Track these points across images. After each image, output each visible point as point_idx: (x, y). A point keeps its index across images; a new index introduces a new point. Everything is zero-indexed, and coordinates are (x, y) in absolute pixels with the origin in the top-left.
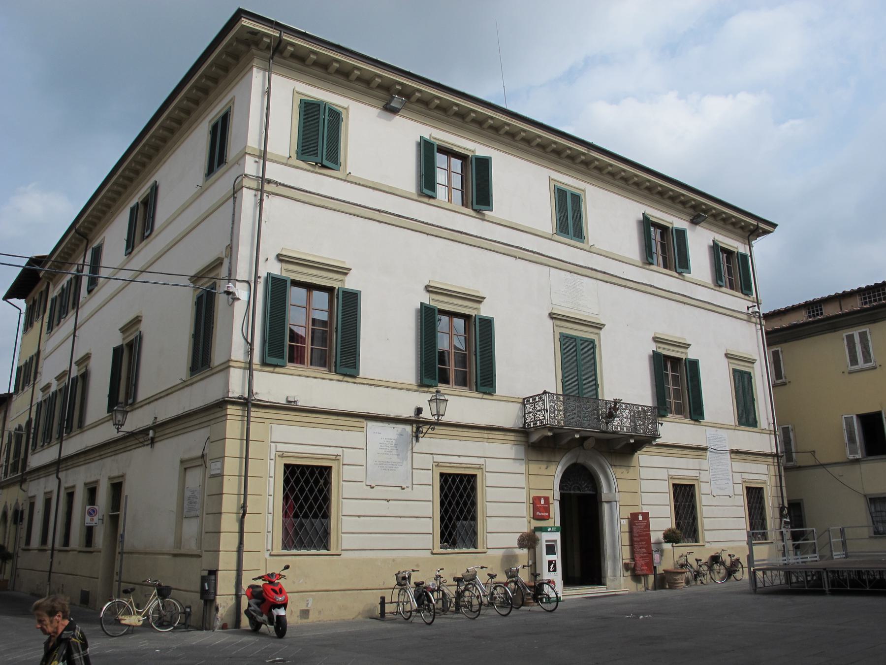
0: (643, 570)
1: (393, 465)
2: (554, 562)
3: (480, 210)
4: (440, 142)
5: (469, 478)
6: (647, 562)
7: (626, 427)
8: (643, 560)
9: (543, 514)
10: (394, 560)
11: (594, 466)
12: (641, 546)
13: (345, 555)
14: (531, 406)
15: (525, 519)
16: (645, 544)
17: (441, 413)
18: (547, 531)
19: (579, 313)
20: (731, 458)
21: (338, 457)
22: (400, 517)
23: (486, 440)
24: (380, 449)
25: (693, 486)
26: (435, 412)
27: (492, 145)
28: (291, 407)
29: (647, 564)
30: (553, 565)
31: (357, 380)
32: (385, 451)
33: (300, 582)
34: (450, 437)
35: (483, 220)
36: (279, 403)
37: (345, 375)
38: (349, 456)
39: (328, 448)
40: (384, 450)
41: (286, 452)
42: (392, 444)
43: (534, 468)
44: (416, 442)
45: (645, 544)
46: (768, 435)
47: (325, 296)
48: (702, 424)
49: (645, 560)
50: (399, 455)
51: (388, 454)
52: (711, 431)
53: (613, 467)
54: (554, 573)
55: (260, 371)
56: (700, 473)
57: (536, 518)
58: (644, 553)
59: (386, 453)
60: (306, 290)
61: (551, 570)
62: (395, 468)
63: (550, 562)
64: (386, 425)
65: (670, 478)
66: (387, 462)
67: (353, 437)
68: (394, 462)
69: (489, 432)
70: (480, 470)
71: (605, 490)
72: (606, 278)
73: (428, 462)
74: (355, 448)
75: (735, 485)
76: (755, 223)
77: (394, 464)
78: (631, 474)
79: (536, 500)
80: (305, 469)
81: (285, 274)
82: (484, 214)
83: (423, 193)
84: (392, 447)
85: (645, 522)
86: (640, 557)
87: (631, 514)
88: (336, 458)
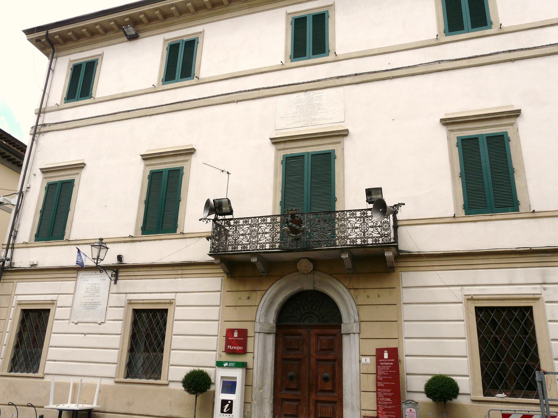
1: (94, 305)
4: (172, 41)
7: (372, 237)
8: (386, 414)
9: (235, 348)
14: (370, 234)
16: (391, 392)
21: (54, 302)
23: (180, 276)
24: (86, 292)
25: (530, 309)
30: (227, 405)
32: (89, 294)
38: (62, 300)
40: (89, 293)
45: (391, 392)
49: (389, 414)
51: (91, 296)
53: (352, 291)
57: (228, 352)
58: (389, 405)
61: (225, 411)
63: (224, 402)
66: (90, 303)
67: (67, 285)
68: (95, 303)
72: (357, 79)
76: (43, 33)
78: (386, 296)
79: (230, 332)
87: (377, 350)
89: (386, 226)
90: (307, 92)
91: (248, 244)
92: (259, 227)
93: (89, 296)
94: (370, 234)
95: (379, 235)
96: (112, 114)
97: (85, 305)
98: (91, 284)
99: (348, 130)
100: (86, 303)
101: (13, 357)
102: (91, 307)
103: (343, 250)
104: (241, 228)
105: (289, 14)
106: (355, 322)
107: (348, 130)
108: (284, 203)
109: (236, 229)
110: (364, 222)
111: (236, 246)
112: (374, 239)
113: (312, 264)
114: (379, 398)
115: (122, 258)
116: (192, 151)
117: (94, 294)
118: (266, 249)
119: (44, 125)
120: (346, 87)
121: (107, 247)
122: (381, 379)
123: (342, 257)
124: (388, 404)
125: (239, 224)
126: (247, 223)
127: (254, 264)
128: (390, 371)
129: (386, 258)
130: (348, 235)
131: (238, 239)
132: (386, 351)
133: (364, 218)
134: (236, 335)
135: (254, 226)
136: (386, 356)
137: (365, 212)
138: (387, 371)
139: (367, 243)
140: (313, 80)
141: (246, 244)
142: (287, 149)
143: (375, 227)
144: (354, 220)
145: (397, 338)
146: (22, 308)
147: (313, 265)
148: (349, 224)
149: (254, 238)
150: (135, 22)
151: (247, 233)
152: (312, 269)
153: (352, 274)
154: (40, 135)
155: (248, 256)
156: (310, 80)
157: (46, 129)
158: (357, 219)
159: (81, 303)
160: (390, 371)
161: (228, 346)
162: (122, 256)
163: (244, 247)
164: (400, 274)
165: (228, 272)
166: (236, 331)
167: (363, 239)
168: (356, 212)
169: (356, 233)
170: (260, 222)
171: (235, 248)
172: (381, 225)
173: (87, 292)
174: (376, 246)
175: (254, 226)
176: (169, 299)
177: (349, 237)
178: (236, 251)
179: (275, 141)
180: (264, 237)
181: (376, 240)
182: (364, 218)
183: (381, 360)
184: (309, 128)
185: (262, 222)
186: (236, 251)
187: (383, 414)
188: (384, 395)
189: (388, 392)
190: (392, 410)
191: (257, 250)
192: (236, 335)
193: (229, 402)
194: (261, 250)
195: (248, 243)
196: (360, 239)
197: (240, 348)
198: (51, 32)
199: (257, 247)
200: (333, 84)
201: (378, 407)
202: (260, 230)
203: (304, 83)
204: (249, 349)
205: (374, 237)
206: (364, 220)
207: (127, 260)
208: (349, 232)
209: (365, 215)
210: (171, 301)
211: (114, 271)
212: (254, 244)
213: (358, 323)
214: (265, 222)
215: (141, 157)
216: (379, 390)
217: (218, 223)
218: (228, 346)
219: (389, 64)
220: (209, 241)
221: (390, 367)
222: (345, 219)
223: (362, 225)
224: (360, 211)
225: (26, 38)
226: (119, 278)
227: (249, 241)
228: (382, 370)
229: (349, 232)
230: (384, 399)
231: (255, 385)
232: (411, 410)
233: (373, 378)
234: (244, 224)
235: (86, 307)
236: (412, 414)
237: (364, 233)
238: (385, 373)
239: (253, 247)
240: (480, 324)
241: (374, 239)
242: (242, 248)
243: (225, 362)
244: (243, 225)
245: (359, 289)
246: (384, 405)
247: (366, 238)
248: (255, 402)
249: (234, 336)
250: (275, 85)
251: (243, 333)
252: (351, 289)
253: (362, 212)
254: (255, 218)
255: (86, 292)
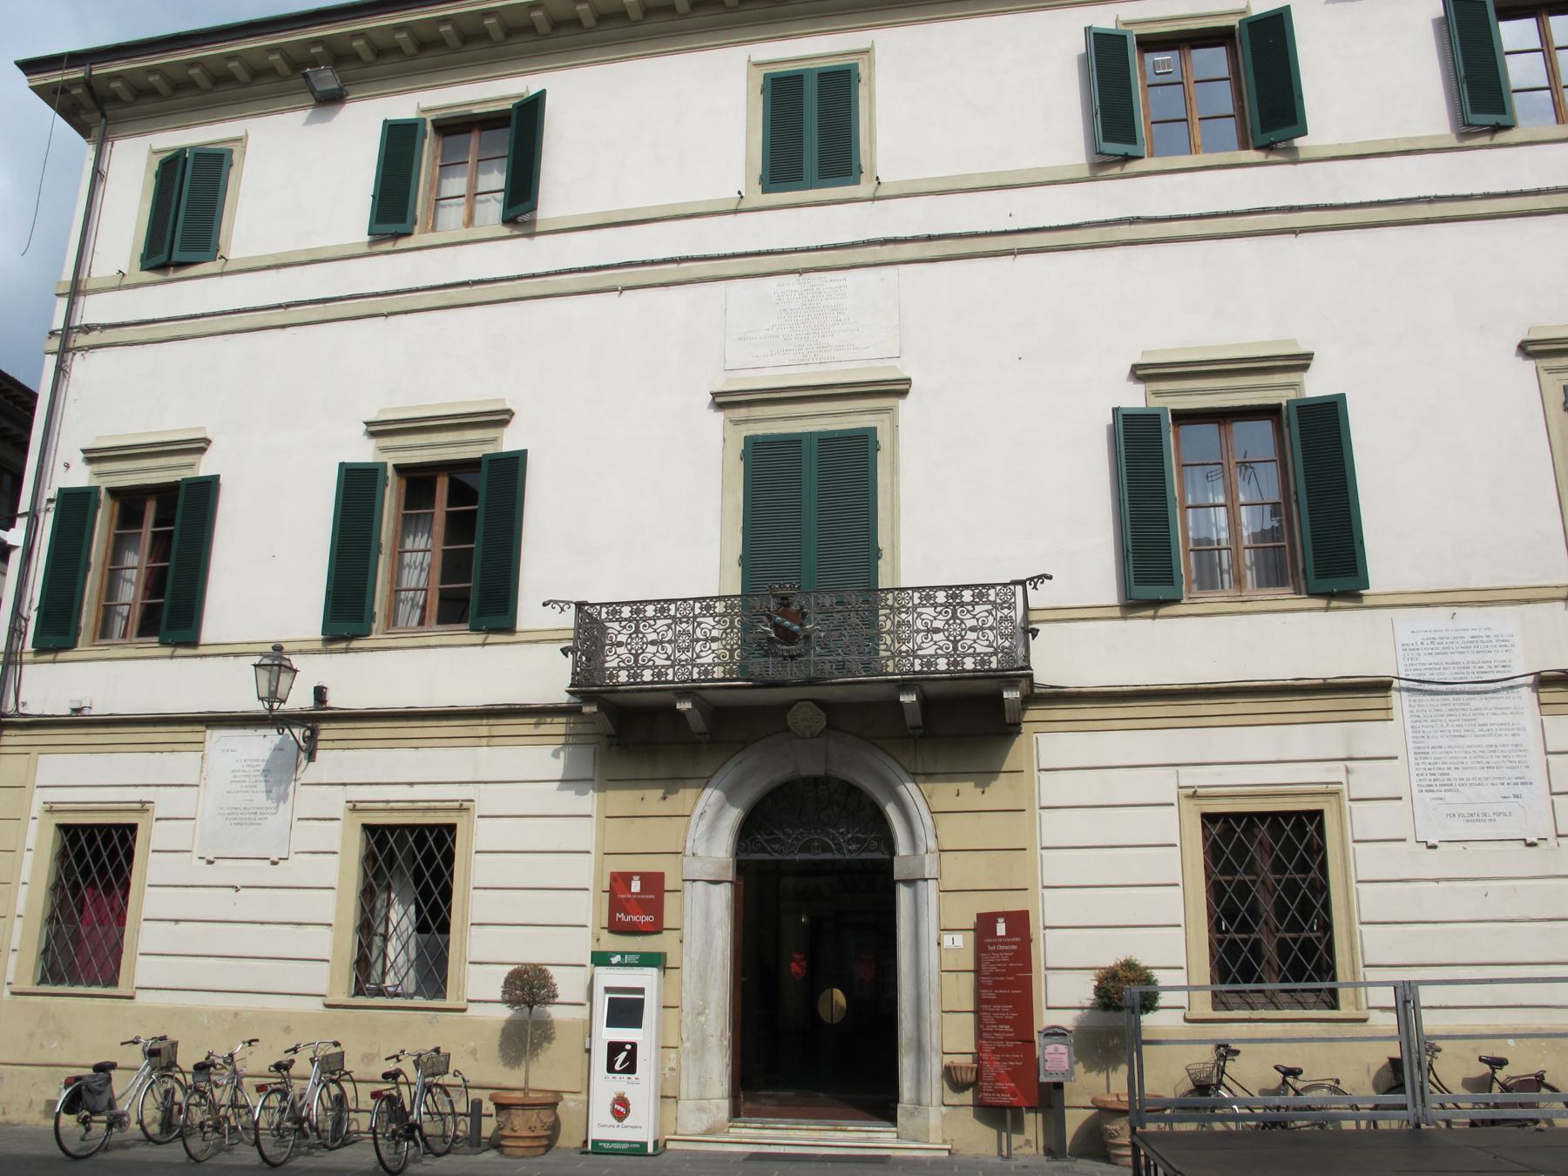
0: (1001, 1091)
2: (628, 1047)
3: (516, 217)
4: (439, 113)
5: (440, 832)
6: (1015, 1067)
7: (973, 655)
8: (1002, 1060)
9: (635, 918)
10: (236, 1014)
11: (865, 784)
12: (999, 1016)
13: (473, 1010)
15: (588, 932)
16: (1011, 1011)
17: (281, 693)
18: (609, 964)
19: (822, 369)
20: (1540, 704)
22: (262, 923)
23: (484, 741)
24: (232, 782)
25: (1316, 816)
26: (264, 693)
27: (663, 47)
28: (78, 721)
29: (1013, 1075)
30: (623, 1055)
31: (201, 650)
32: (242, 787)
33: (53, 1046)
34: (1076, 726)
35: (1296, 162)
36: (53, 716)
37: (1330, 596)
38: (164, 802)
39: (133, 789)
40: (240, 784)
41: (1199, 787)
42: (257, 771)
43: (623, 799)
44: (309, 761)
45: (1011, 1011)
46: (24, 666)
47: (1265, 427)
48: (1366, 601)
50: (271, 792)
51: (247, 792)
52: (1410, 624)
54: (627, 1076)
55: (35, 663)
56: (1348, 771)
58: (1006, 1039)
59: (245, 789)
60: (1216, 426)
61: (617, 1067)
62: (261, 819)
63: (614, 1048)
64: (249, 732)
65: (1187, 797)
66: (245, 808)
68: (258, 808)
69: (492, 722)
70: (1333, 799)
71: (902, 847)
73: (336, 801)
74: (182, 785)
75: (1555, 797)
76: (77, 74)
77: (259, 811)
78: (1000, 791)
79: (620, 880)
80: (445, 831)
81: (1156, 403)
82: (1295, 149)
83: (1470, 125)
84: (255, 776)
85: (1014, 943)
86: (993, 1052)
88: (143, 807)
89: (1006, 628)
90: (805, 276)
91: (668, 667)
92: (696, 624)
93: (242, 791)
94: (970, 647)
95: (991, 650)
96: (280, 306)
97: (233, 813)
98: (245, 761)
99: (910, 380)
100: (234, 811)
101: (43, 946)
102: (250, 819)
103: (905, 685)
104: (650, 626)
105: (757, 65)
106: (927, 852)
107: (910, 380)
108: (751, 561)
109: (637, 627)
110: (954, 617)
111: (638, 671)
112: (979, 658)
113: (823, 714)
114: (985, 1025)
115: (325, 693)
116: (506, 417)
117: (255, 786)
118: (714, 680)
119: (88, 329)
120: (902, 268)
121: (295, 667)
122: (990, 983)
123: (901, 700)
124: (1005, 1037)
125: (645, 616)
126: (665, 614)
127: (681, 715)
128: (1011, 965)
129: (1003, 703)
130: (916, 648)
131: (643, 653)
132: (1001, 920)
133: (954, 607)
134: (636, 886)
135: (684, 622)
136: (1001, 929)
137: (957, 592)
138: (1004, 965)
139: (949, 660)
140: (819, 244)
141: (663, 667)
142: (755, 420)
143: (982, 629)
144: (931, 610)
145: (197, 783)
146: (57, 822)
147: (827, 718)
148: (919, 621)
149: (683, 651)
150: (339, 55)
151: (666, 639)
152: (822, 727)
153: (921, 737)
154: (76, 356)
155: (669, 696)
156: (813, 244)
157: (94, 338)
158: (939, 609)
159: (221, 809)
160: (1011, 965)
161: (618, 915)
162: (326, 688)
163: (659, 674)
164: (1034, 738)
165: (613, 732)
166: (636, 878)
167: (952, 659)
168: (935, 592)
169: (935, 643)
170: (697, 611)
171: (635, 676)
172: (994, 625)
173: (235, 782)
174: (991, 675)
175: (684, 622)
176: (457, 801)
177: (919, 652)
178: (638, 683)
179: (723, 402)
180: (710, 649)
181: (983, 662)
182: (954, 607)
183: (990, 940)
184: (812, 368)
185: (705, 612)
186: (638, 683)
187: (992, 1061)
188: (995, 1019)
189: (1005, 1012)
190: (1014, 1050)
191: (693, 681)
192: (636, 886)
193: (628, 1047)
194: (703, 681)
195: (669, 663)
196: (946, 658)
197: (647, 919)
198: (100, 70)
199: (691, 674)
200: (871, 260)
201: (979, 1047)
202: (698, 630)
203: (796, 251)
204: (668, 921)
205: (979, 654)
206: (954, 612)
207: (335, 701)
208: (919, 640)
209: (958, 601)
210: (464, 803)
211: (308, 728)
212: (683, 666)
213: (937, 855)
214: (711, 612)
215: (365, 426)
216: (985, 1006)
217: (589, 611)
218: (618, 915)
219: (1011, 215)
220: (567, 657)
221: (1010, 954)
222: (908, 608)
223: (949, 625)
224: (945, 591)
225: (27, 84)
226: (320, 745)
227: (672, 658)
228: (991, 963)
229: (919, 640)
230: (996, 1026)
231: (686, 1006)
232: (1056, 1049)
233: (969, 979)
234: (659, 615)
235: (235, 819)
236: (1058, 1056)
237: (955, 642)
238: (999, 968)
239: (683, 674)
240: (1213, 852)
241: (979, 658)
242: (653, 675)
243: (613, 952)
244: (655, 619)
245: (938, 774)
246: (995, 1040)
247: (959, 656)
248: (687, 1045)
249: (633, 891)
250: (722, 252)
251: (654, 882)
252: (917, 774)
253: (951, 592)
254: (685, 600)
255: (232, 782)
